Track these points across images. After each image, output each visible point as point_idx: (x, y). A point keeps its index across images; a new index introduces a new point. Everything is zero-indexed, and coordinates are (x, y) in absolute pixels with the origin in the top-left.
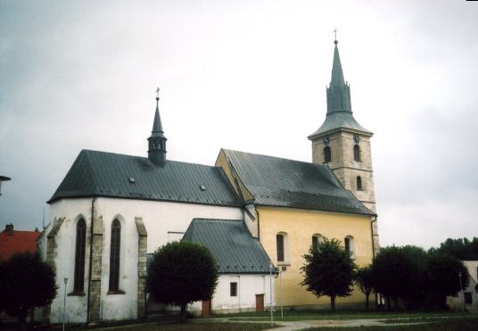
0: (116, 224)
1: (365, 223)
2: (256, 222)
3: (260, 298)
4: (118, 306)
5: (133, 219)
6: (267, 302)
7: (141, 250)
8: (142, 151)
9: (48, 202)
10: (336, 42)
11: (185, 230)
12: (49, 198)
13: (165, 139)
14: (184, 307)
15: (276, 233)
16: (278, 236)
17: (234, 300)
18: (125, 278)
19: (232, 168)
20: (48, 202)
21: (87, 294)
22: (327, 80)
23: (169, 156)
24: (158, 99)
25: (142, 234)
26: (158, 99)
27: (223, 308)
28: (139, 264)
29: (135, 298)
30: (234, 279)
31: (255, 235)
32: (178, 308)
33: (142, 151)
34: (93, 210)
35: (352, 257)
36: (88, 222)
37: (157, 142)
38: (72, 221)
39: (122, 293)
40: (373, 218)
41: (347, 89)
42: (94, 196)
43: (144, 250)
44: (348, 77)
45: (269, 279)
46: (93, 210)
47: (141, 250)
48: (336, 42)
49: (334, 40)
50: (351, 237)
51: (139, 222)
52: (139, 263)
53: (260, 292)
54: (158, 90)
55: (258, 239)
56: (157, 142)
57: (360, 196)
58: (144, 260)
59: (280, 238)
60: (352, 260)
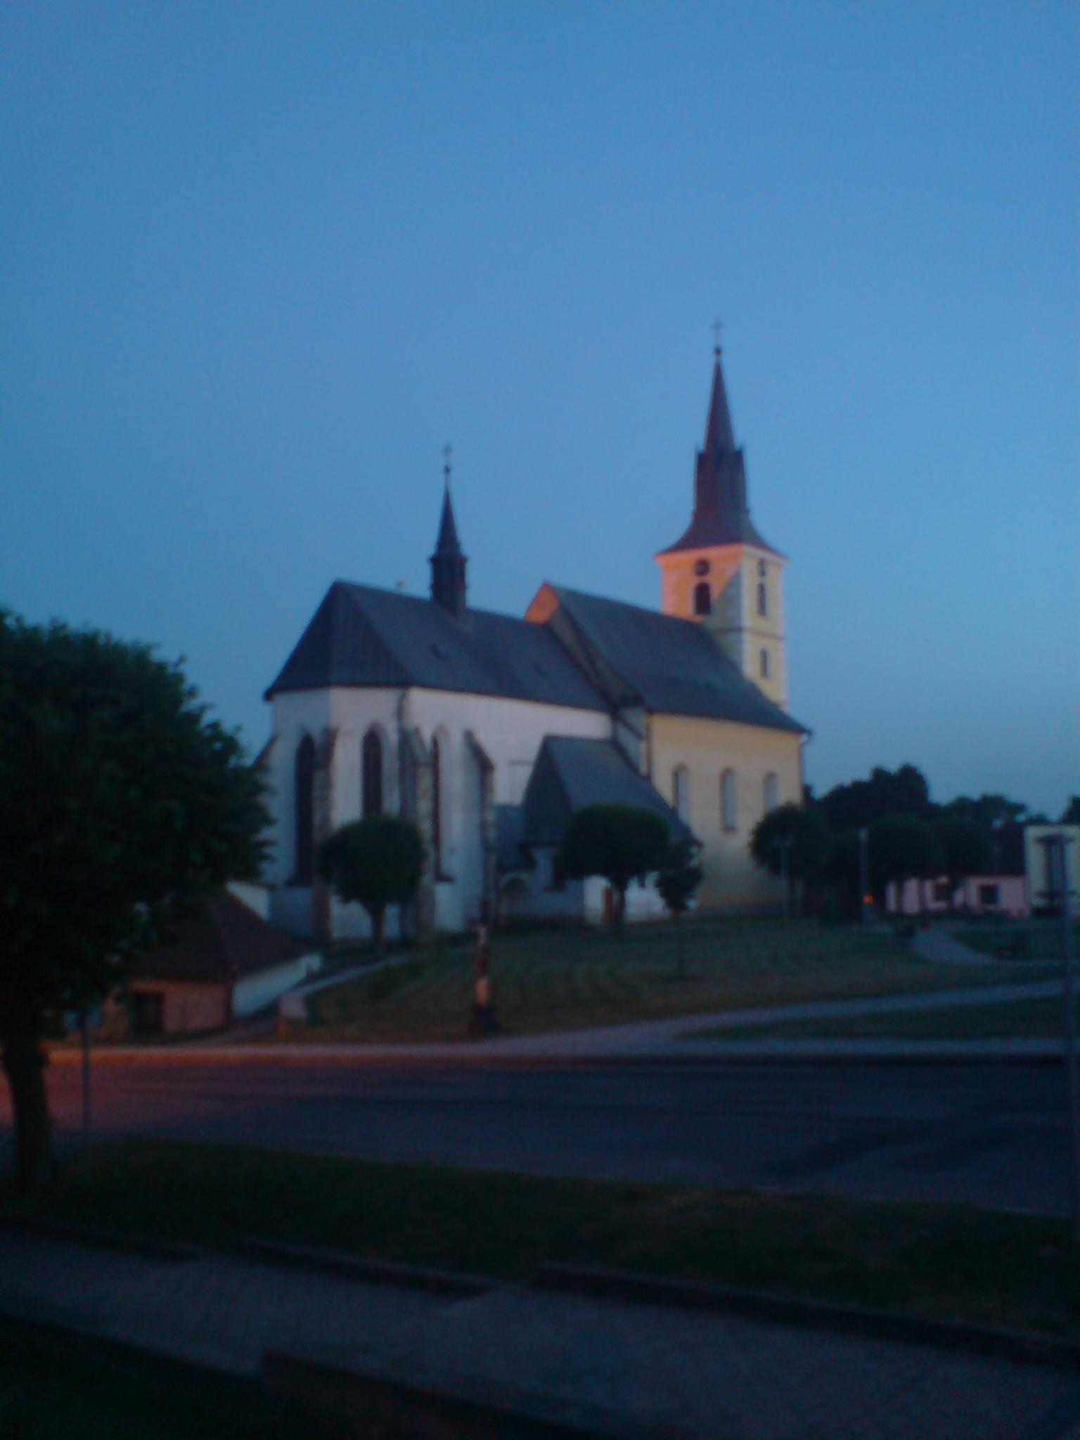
1: (781, 743)
4: (449, 905)
10: (718, 351)
12: (271, 670)
19: (574, 624)
22: (697, 437)
25: (482, 764)
28: (483, 825)
33: (419, 584)
34: (400, 712)
35: (191, 705)
36: (391, 739)
37: (448, 564)
40: (804, 738)
41: (738, 456)
42: (402, 681)
44: (743, 432)
46: (400, 712)
48: (718, 351)
56: (448, 564)
58: (491, 816)
60: (193, 718)
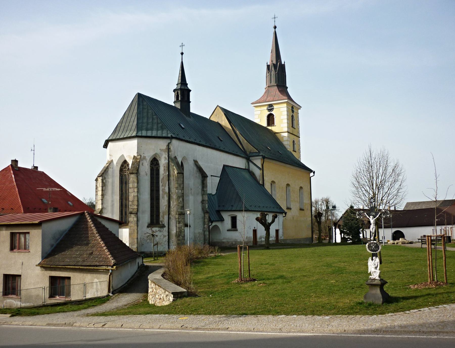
2: (261, 171)
8: (170, 99)
10: (275, 27)
13: (190, 91)
23: (193, 109)
24: (182, 54)
26: (182, 54)
28: (203, 202)
31: (261, 182)
34: (169, 149)
37: (183, 93)
48: (275, 27)
53: (277, 228)
54: (182, 46)
55: (263, 185)
56: (183, 93)
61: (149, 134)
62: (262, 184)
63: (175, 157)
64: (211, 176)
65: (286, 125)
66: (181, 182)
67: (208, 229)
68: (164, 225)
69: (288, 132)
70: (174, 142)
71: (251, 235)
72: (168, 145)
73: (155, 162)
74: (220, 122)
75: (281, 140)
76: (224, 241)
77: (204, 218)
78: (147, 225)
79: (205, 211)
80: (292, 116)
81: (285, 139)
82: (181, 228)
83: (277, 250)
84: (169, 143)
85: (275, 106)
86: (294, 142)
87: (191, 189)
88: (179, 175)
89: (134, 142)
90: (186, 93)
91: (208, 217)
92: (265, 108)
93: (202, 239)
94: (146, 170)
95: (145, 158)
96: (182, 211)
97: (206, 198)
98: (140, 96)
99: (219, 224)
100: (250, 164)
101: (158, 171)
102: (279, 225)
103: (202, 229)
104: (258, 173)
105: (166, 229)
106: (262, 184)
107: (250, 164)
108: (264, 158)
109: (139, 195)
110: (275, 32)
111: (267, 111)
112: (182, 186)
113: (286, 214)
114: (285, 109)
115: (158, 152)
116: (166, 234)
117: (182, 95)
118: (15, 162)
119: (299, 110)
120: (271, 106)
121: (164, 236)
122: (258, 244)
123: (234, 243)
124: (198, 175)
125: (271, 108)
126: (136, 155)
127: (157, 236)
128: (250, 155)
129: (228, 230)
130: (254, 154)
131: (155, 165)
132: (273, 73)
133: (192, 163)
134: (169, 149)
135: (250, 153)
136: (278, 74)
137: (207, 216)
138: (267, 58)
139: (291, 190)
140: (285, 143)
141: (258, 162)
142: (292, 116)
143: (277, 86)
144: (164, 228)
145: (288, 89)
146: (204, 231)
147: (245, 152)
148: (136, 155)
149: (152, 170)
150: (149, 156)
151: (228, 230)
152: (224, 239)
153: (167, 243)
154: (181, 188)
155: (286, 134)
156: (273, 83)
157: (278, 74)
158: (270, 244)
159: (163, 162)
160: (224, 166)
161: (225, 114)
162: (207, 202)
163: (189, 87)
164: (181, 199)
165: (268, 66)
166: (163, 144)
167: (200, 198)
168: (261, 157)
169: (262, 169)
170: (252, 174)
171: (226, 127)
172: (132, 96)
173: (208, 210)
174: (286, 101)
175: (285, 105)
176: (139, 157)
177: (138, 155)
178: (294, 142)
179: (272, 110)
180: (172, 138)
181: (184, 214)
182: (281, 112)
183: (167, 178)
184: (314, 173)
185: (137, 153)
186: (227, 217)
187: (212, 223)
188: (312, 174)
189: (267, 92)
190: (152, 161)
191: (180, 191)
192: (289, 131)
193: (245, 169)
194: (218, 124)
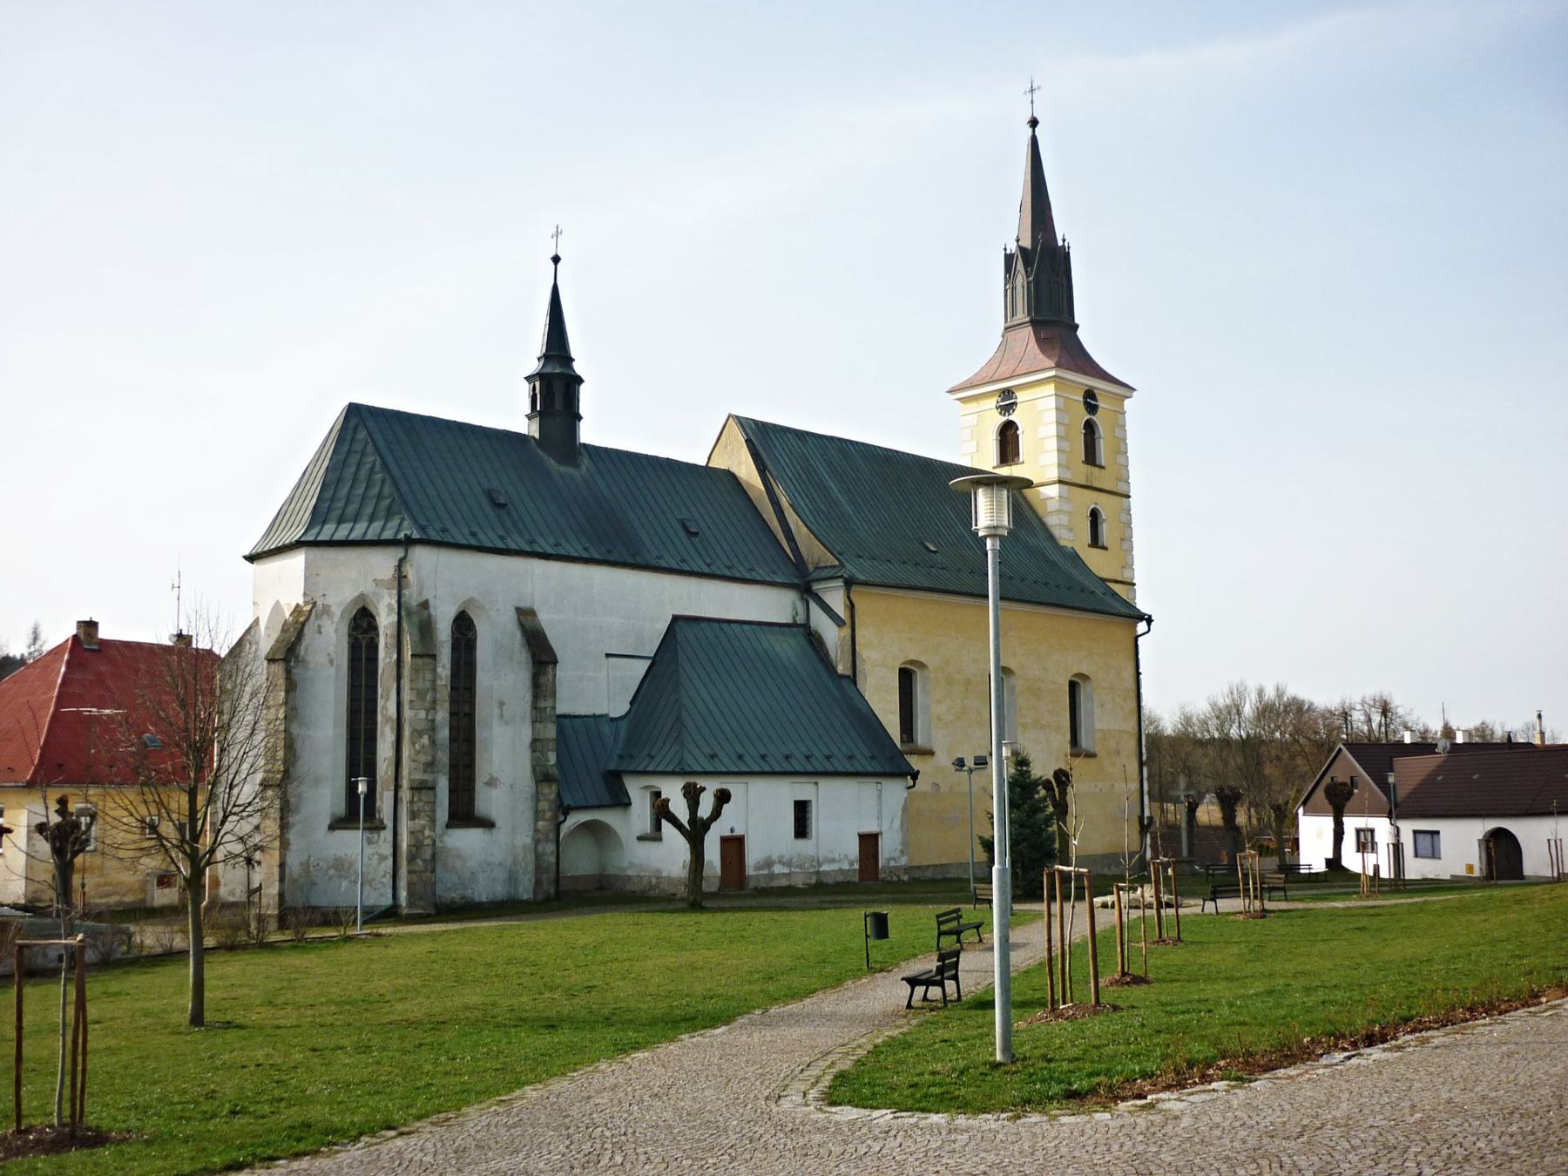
0: (463, 625)
2: (847, 631)
3: (869, 842)
5: (512, 615)
6: (889, 849)
7: (542, 704)
8: (510, 410)
9: (246, 558)
10: (1034, 123)
11: (651, 649)
13: (579, 380)
14: (985, 537)
15: (897, 665)
16: (1073, 687)
17: (802, 844)
18: (492, 782)
20: (246, 558)
21: (389, 823)
23: (590, 433)
24: (556, 259)
25: (540, 652)
26: (556, 259)
27: (778, 869)
28: (536, 744)
29: (525, 839)
30: (802, 789)
31: (842, 668)
32: (989, 542)
33: (510, 410)
34: (400, 579)
37: (557, 387)
38: (337, 611)
39: (487, 824)
43: (549, 703)
44: (1063, 229)
45: (895, 791)
47: (542, 704)
48: (1034, 123)
49: (1028, 118)
50: (1085, 677)
51: (528, 621)
52: (535, 741)
53: (871, 828)
54: (557, 234)
55: (853, 679)
56: (557, 387)
57: (1097, 562)
59: (906, 677)
61: (341, 535)
62: (849, 673)
63: (425, 605)
64: (608, 655)
65: (1053, 458)
66: (428, 684)
67: (552, 835)
68: (382, 821)
69: (1060, 482)
70: (420, 555)
71: (853, 849)
72: (399, 567)
73: (362, 621)
74: (734, 470)
75: (1040, 511)
76: (630, 872)
77: (537, 797)
78: (328, 822)
79: (542, 777)
80: (1090, 427)
81: (1052, 506)
82: (422, 832)
83: (767, 915)
84: (401, 561)
85: (1021, 396)
86: (1094, 515)
87: (502, 704)
88: (419, 661)
89: (296, 562)
90: (559, 390)
91: (553, 797)
92: (992, 402)
93: (531, 867)
94: (331, 649)
95: (326, 610)
96: (426, 777)
97: (551, 731)
98: (355, 413)
99: (610, 818)
100: (813, 606)
101: (373, 647)
102: (880, 818)
103: (530, 833)
104: (832, 635)
105: (387, 834)
106: (849, 673)
107: (813, 605)
108: (849, 583)
109: (295, 729)
110: (1034, 142)
111: (996, 412)
112: (429, 697)
113: (915, 776)
114: (1051, 403)
115: (367, 587)
116: (389, 851)
117: (559, 390)
118: (90, 626)
119: (1127, 402)
120: (1008, 393)
121: (382, 858)
122: (752, 885)
123: (654, 881)
124: (522, 657)
125: (1007, 400)
126: (301, 603)
127: (259, 863)
128: (815, 575)
129: (640, 838)
130: (824, 574)
131: (365, 632)
132: (1020, 280)
133: (508, 619)
134: (400, 579)
135: (817, 568)
136: (1043, 279)
137: (550, 791)
138: (1011, 230)
139: (1019, 689)
140: (1051, 521)
141: (836, 599)
142: (1090, 427)
143: (1032, 322)
144: (382, 833)
145: (1079, 333)
146: (537, 842)
147: (799, 564)
148: (301, 603)
149: (354, 647)
150: (340, 599)
151: (640, 838)
152: (632, 865)
153: (388, 880)
154: (427, 705)
155: (1053, 491)
156: (1022, 316)
157: (1043, 279)
158: (703, 893)
159: (385, 620)
160: (676, 619)
161: (748, 441)
162: (552, 745)
163: (579, 368)
164: (425, 740)
165: (1009, 259)
166: (382, 563)
167: (526, 734)
168: (840, 583)
169: (850, 623)
170: (814, 641)
171: (753, 487)
172: (331, 415)
173: (555, 771)
174: (1052, 373)
175: (1050, 389)
176: (308, 608)
177: (306, 603)
178: (1094, 515)
179: (1007, 409)
180: (409, 542)
181: (433, 788)
182: (1042, 415)
183: (394, 673)
184: (1149, 621)
185: (305, 594)
186: (636, 789)
187: (566, 814)
188: (1142, 627)
189: (1004, 347)
190: (355, 619)
191: (422, 714)
192: (1068, 477)
193: (794, 625)
194: (730, 476)
